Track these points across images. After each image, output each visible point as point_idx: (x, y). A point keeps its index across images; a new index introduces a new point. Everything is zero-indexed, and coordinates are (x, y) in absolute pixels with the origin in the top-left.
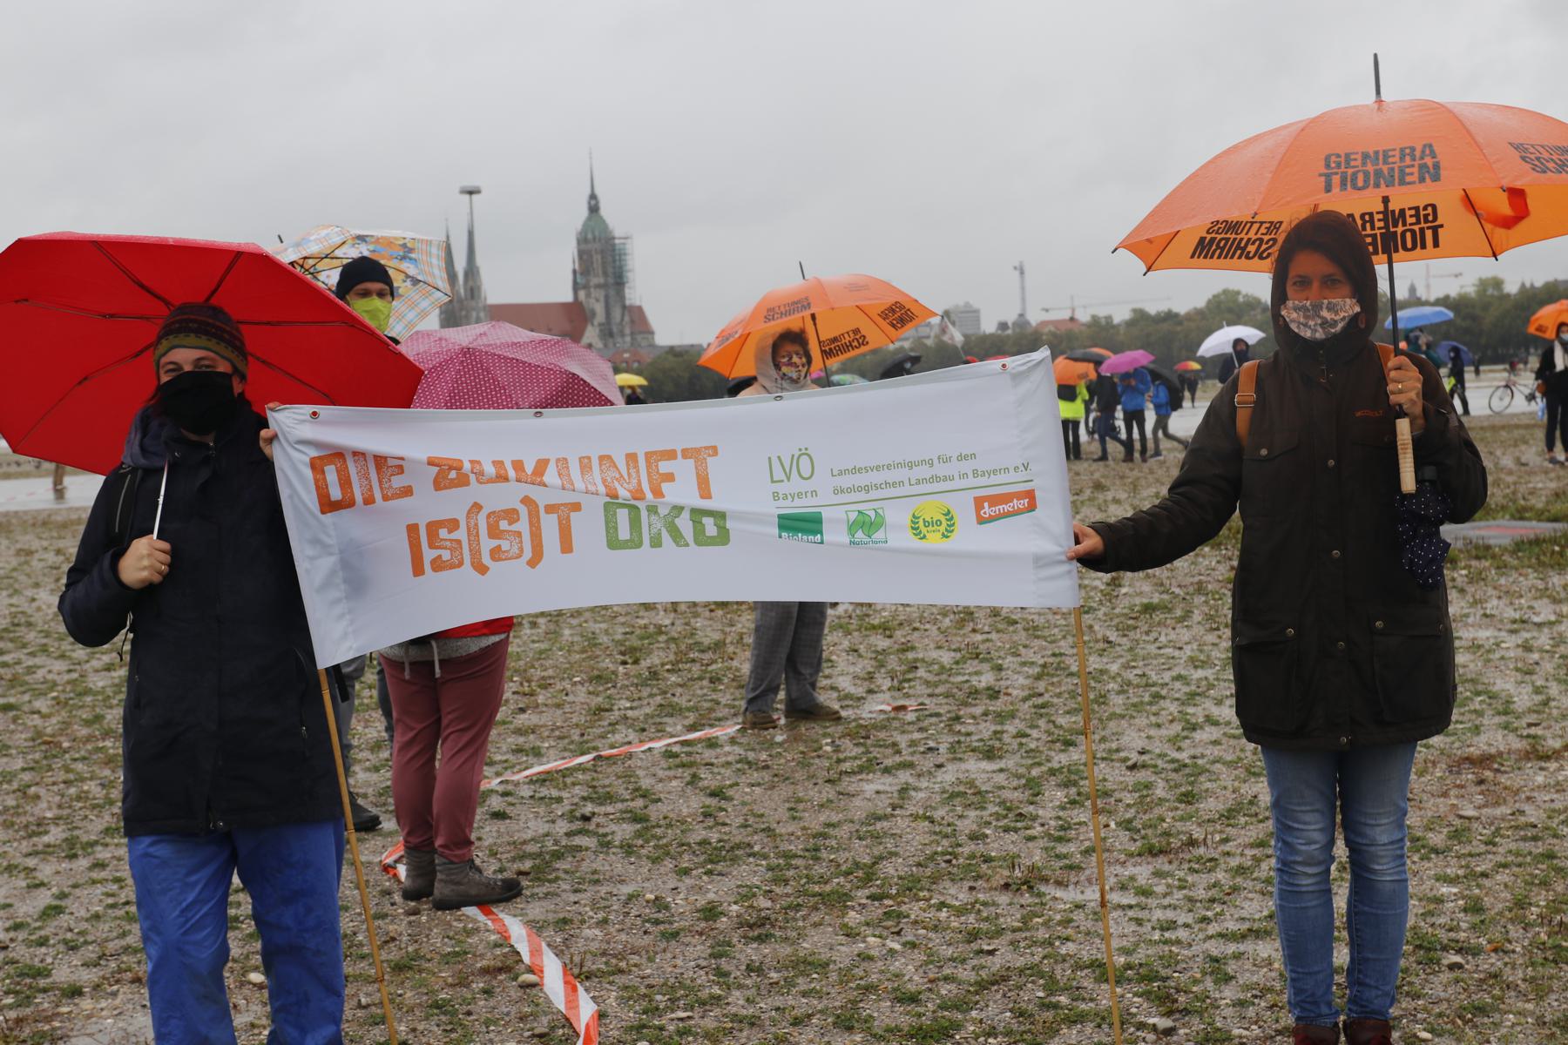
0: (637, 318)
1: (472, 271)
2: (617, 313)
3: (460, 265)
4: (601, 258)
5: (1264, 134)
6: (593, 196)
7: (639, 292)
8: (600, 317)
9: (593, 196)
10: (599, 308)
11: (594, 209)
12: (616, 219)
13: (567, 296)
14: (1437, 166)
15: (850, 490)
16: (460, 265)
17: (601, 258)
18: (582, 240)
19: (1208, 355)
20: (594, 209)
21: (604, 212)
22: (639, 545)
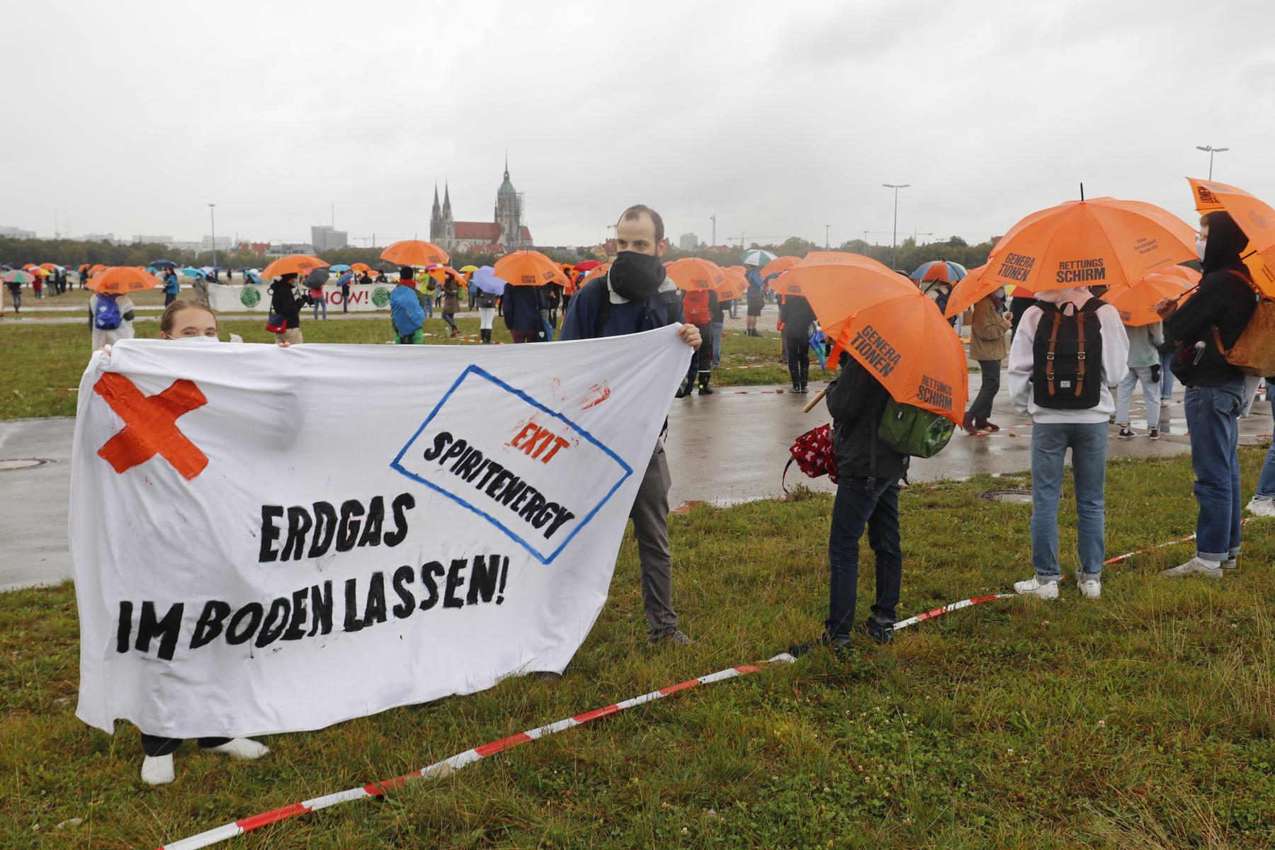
0: (525, 233)
1: (447, 205)
2: (515, 230)
3: (441, 202)
4: (508, 201)
5: (443, 699)
6: (506, 172)
7: (526, 219)
8: (507, 231)
9: (506, 172)
10: (507, 226)
11: (507, 179)
12: (517, 184)
13: (492, 220)
14: (1103, 270)
15: (749, 468)
16: (441, 202)
17: (508, 201)
18: (500, 193)
19: (274, 524)
20: (507, 179)
21: (511, 180)
22: (290, 510)
